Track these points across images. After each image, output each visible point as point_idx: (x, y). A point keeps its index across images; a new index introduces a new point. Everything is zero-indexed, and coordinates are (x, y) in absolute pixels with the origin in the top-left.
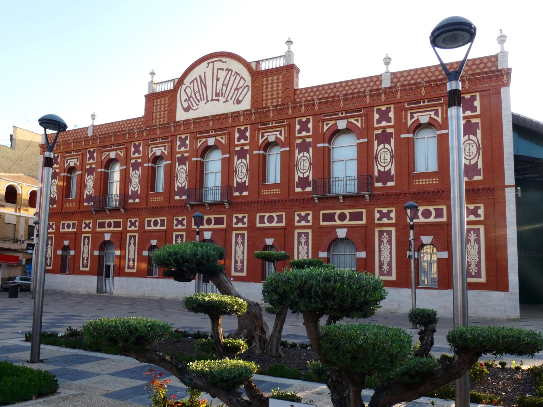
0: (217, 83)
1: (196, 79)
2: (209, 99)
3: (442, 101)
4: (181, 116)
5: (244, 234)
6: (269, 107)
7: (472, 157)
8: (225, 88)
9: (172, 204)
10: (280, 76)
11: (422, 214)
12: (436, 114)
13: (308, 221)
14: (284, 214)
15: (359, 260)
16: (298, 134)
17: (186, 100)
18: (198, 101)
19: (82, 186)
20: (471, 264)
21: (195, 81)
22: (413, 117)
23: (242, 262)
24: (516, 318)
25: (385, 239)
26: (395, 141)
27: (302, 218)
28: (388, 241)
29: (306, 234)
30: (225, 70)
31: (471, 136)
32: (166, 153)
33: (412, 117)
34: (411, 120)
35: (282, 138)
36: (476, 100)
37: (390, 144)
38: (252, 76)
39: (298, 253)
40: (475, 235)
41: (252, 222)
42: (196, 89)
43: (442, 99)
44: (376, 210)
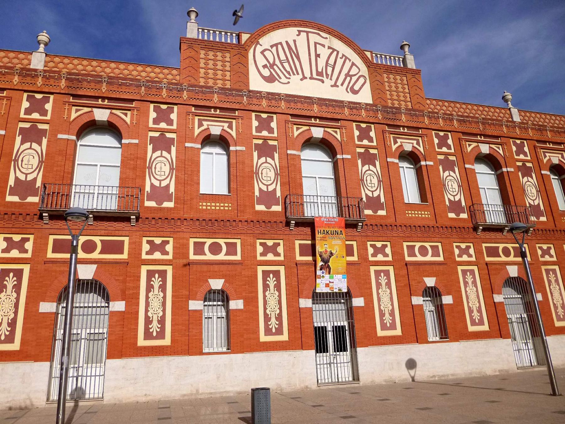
2: (308, 74)
3: (4, 95)
5: (165, 272)
7: (164, 177)
8: (330, 70)
11: (220, 246)
12: (230, 127)
13: (386, 255)
14: (238, 242)
15: (112, 314)
17: (265, 66)
23: (479, 311)
25: (272, 282)
26: (48, 141)
28: (275, 286)
29: (387, 273)
31: (164, 152)
32: (234, 133)
33: (200, 125)
34: (394, 144)
38: (368, 67)
39: (164, 304)
41: (181, 250)
42: (283, 57)
44: (145, 239)
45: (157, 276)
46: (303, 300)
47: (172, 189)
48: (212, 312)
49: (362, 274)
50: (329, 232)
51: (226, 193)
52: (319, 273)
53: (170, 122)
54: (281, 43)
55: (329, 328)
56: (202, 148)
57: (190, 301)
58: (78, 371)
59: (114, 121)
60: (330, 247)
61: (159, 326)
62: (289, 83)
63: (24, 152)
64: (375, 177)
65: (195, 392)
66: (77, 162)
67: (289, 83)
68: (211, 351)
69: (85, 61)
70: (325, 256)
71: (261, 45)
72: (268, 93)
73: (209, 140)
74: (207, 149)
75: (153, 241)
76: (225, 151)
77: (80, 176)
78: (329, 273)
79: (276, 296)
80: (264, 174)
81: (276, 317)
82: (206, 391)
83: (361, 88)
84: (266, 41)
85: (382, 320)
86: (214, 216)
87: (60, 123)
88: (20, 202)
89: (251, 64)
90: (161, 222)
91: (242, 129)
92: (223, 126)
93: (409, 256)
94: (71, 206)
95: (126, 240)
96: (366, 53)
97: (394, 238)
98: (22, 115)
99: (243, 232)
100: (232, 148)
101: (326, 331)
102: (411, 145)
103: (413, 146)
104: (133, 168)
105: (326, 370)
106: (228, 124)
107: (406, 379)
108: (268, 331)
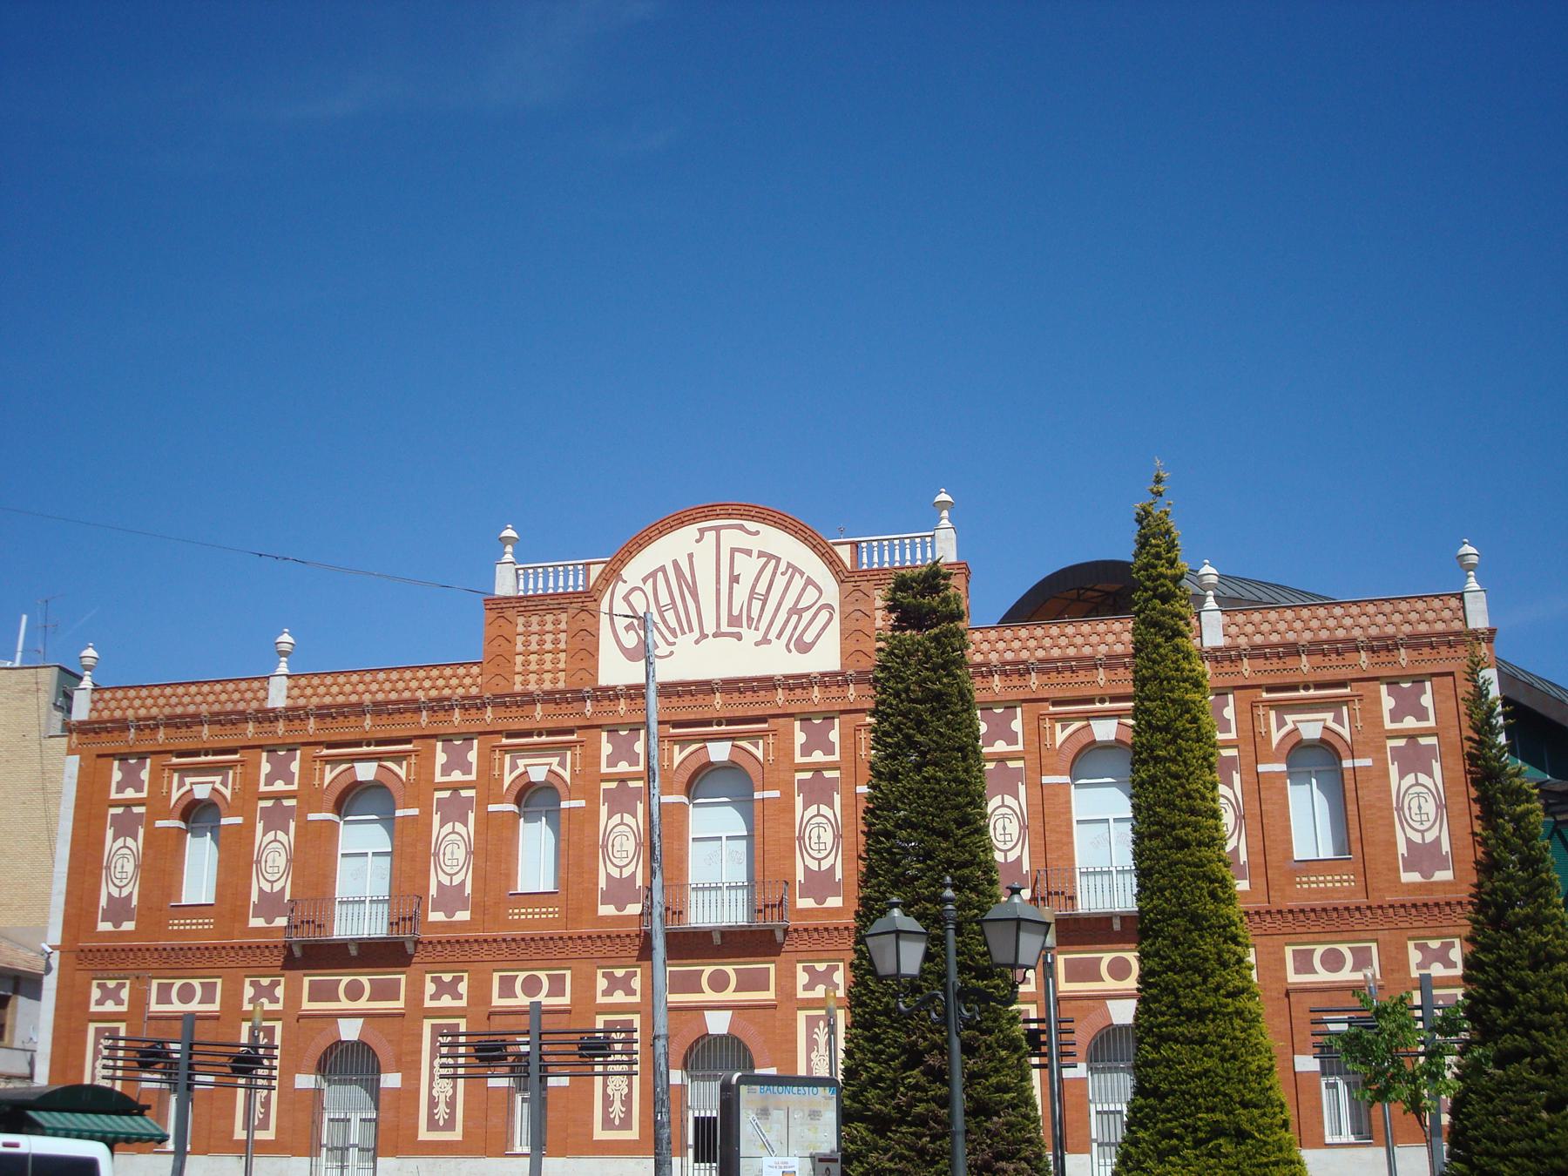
0: (731, 588)
1: (663, 569)
2: (710, 628)
4: (615, 670)
8: (757, 605)
11: (1323, 963)
19: (1038, 825)
21: (660, 574)
22: (1286, 724)
30: (755, 554)
32: (567, 775)
33: (514, 767)
42: (664, 599)
53: (1421, 714)
54: (663, 569)
80: (448, 856)
83: (818, 636)
84: (635, 570)
85: (606, 1113)
90: (457, 950)
93: (1297, 971)
104: (410, 857)
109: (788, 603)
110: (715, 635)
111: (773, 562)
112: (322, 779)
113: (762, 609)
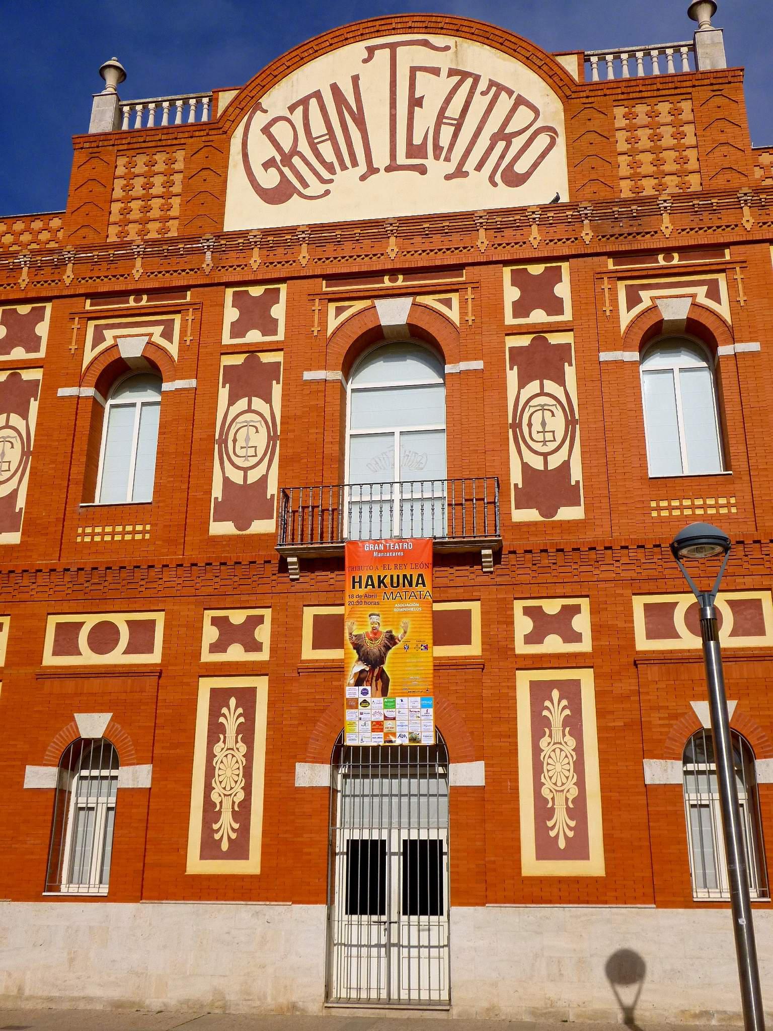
1: (318, 95)
2: (381, 159)
4: (244, 211)
5: (253, 691)
6: (130, 243)
8: (447, 132)
9: (192, 554)
10: (180, 155)
12: (714, 294)
13: (574, 637)
15: (458, 795)
16: (233, 336)
17: (269, 164)
18: (330, 168)
20: (553, 809)
21: (313, 102)
22: (639, 301)
24: (734, 1013)
27: (229, 634)
29: (571, 691)
32: (173, 349)
33: (99, 338)
34: (629, 308)
35: (173, 349)
36: (560, 280)
37: (268, 400)
38: (566, 99)
40: (565, 702)
41: (612, 631)
42: (318, 128)
43: (727, 251)
44: (209, 614)
45: (555, 694)
46: (307, 765)
47: (576, 474)
48: (697, 791)
49: (486, 693)
50: (387, 581)
51: (715, 467)
52: (352, 692)
53: (555, 306)
54: (318, 95)
55: (395, 846)
56: (644, 357)
57: (29, 769)
58: (388, 930)
59: (424, 323)
60: (386, 622)
61: (572, 824)
62: (327, 192)
63: (531, 403)
64: (559, 413)
65: (14, 992)
66: (348, 432)
67: (327, 192)
68: (83, 891)
69: (56, 219)
70: (374, 648)
71: (265, 111)
72: (266, 232)
73: (658, 337)
74: (657, 361)
75: (226, 618)
76: (705, 359)
77: (358, 464)
78: (384, 693)
79: (240, 756)
80: (241, 442)
81: (233, 812)
82: (40, 994)
83: (535, 165)
84: (276, 100)
85: (541, 829)
86: (557, 538)
87: (305, 345)
88: (238, 536)
89: (235, 166)
90: (560, 561)
91: (745, 293)
92: (693, 296)
93: (651, 635)
94: (345, 535)
95: (475, 607)
96: (561, 60)
97: (602, 585)
98: (226, 339)
99: (173, 592)
100: (724, 350)
101: (383, 854)
102: (690, 300)
103: (694, 304)
104: (477, 432)
105: (374, 961)
106: (705, 288)
107: (605, 1014)
108: (210, 849)
109: (493, 126)
110: (388, 169)
111: (469, 81)
112: (324, 323)
113: (455, 135)
